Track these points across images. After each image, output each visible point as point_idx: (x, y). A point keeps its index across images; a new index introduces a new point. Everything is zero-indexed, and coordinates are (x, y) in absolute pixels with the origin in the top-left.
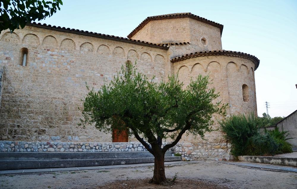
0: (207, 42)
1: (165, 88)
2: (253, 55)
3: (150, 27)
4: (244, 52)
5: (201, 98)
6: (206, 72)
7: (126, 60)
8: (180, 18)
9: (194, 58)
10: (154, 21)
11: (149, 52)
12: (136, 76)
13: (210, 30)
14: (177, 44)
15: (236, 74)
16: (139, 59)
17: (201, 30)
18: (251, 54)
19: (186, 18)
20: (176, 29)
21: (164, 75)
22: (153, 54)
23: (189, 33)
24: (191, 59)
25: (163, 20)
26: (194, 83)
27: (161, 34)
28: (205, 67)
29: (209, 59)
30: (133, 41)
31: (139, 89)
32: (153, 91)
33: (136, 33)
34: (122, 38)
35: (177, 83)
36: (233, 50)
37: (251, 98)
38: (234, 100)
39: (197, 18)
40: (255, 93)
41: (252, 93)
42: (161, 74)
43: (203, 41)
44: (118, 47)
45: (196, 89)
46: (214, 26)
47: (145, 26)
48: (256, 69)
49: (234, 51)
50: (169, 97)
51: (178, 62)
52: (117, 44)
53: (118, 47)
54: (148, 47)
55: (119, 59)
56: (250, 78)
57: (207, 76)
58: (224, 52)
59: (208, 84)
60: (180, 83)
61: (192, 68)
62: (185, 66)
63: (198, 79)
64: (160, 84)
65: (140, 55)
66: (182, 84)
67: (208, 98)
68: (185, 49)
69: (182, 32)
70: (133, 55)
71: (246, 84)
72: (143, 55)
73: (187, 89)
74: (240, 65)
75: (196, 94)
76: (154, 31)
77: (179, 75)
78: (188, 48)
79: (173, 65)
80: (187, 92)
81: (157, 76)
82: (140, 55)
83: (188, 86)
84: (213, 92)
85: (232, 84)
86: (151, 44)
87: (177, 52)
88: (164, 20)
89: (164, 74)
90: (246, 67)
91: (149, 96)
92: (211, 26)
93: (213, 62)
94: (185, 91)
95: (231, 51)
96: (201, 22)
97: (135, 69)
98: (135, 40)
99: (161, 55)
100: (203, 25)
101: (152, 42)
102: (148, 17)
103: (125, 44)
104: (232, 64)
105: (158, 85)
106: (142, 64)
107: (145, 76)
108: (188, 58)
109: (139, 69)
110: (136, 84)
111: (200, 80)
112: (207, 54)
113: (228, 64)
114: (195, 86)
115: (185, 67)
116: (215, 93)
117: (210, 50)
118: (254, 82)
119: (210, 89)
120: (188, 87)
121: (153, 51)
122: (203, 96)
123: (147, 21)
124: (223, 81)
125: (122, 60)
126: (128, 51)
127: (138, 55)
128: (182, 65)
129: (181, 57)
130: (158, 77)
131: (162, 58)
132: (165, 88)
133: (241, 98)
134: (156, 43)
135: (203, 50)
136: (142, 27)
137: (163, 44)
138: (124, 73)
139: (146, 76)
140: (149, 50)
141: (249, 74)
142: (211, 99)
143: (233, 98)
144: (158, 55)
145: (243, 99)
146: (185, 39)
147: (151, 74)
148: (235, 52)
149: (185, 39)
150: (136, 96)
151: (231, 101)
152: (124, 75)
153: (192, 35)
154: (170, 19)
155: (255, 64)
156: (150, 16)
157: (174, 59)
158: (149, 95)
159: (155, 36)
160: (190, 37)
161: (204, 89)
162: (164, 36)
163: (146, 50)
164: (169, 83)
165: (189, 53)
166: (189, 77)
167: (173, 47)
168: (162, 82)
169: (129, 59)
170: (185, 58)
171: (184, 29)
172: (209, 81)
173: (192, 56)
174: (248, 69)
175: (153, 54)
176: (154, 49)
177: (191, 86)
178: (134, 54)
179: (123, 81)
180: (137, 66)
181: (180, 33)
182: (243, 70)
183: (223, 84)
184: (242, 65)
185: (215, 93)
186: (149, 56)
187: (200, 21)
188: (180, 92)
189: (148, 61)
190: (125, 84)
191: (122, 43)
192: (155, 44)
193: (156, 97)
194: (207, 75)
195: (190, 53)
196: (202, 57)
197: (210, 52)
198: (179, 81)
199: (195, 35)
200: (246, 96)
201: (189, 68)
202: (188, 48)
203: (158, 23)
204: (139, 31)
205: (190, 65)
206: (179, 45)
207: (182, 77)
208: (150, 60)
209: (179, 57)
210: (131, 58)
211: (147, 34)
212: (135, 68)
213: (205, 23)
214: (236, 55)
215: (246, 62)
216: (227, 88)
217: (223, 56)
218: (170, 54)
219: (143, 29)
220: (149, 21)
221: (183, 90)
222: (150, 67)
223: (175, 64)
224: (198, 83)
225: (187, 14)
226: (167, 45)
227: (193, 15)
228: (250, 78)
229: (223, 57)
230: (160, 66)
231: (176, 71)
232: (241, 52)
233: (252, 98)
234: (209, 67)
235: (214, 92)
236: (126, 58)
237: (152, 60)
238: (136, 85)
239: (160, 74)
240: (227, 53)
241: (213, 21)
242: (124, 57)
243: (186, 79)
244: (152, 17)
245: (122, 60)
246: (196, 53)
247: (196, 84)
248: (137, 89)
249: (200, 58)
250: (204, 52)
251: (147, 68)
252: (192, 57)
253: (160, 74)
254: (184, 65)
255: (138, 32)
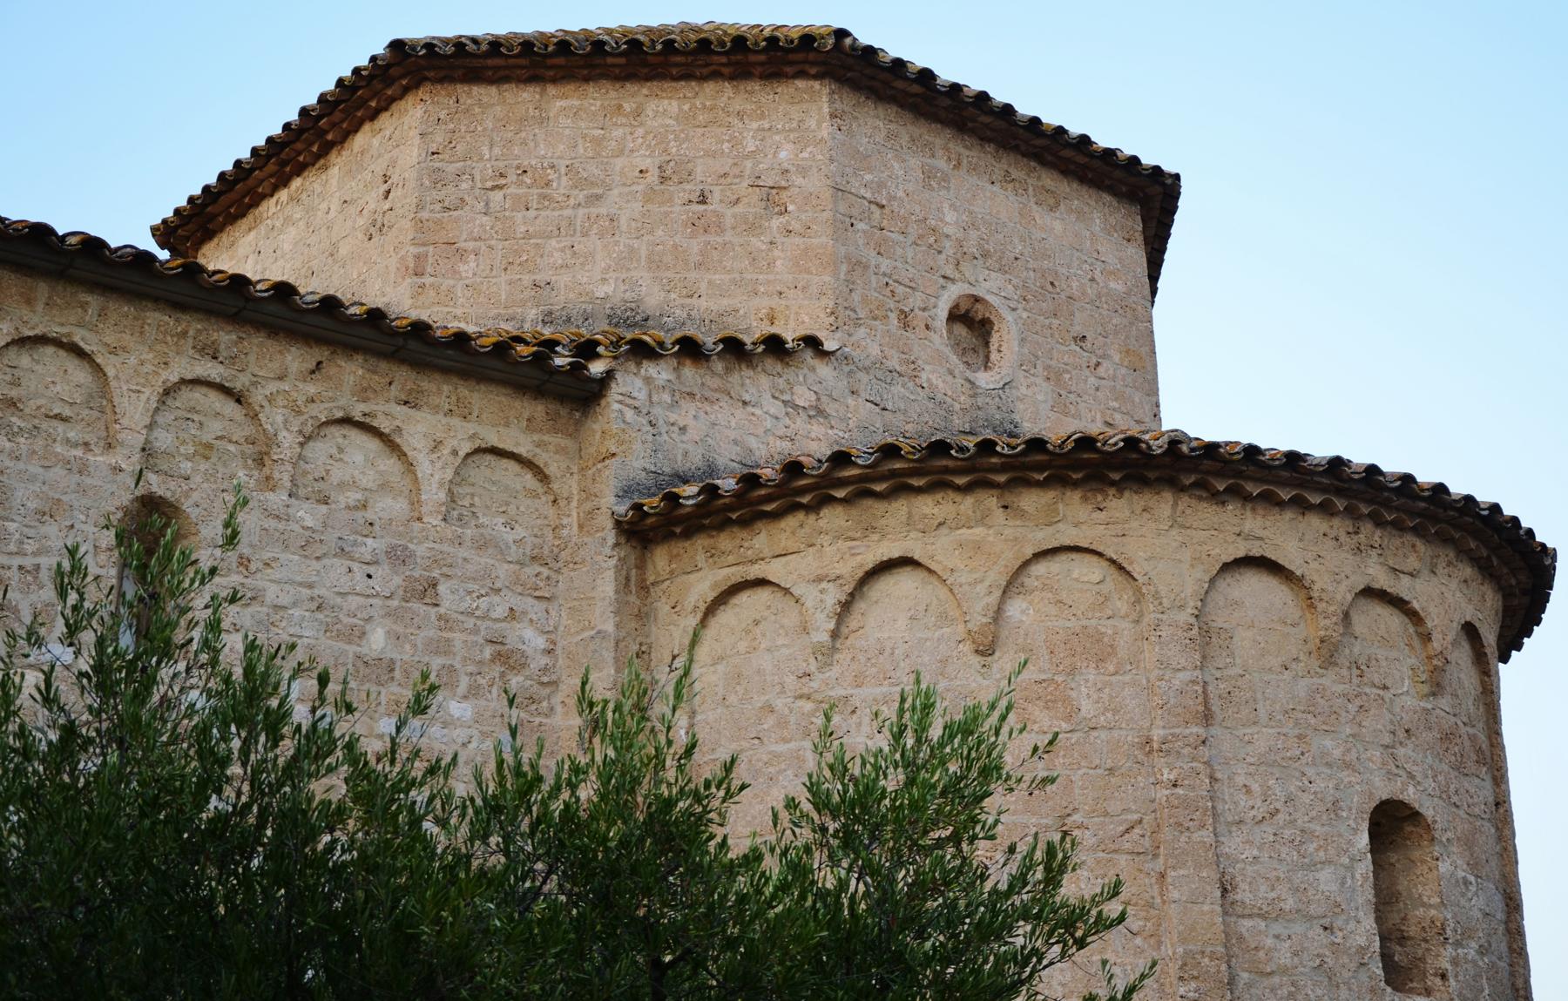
0: (1007, 340)
1: (544, 817)
2: (1484, 496)
3: (411, 155)
4: (1391, 464)
5: (922, 936)
6: (986, 651)
7: (121, 495)
8: (732, 78)
9: (869, 502)
10: (461, 89)
11: (388, 413)
12: (227, 680)
13: (1041, 216)
14: (690, 349)
15: (1302, 688)
16: (269, 483)
17: (950, 217)
18: (1457, 488)
19: (800, 83)
20: (691, 188)
21: (545, 670)
22: (437, 445)
23: (822, 239)
24: (832, 517)
25: (552, 90)
26: (856, 770)
27: (527, 235)
28: (981, 603)
29: (1022, 514)
30: (215, 288)
31: (252, 820)
32: (409, 850)
33: (255, 204)
34: (93, 246)
35: (671, 775)
36: (1275, 438)
37: (1471, 950)
38: (1284, 971)
39: (916, 89)
40: (1512, 904)
41: (1481, 901)
42: (508, 659)
43: (961, 330)
44: (42, 340)
45: (873, 838)
46: (1083, 180)
47: (360, 140)
48: (1511, 641)
49: (1285, 446)
50: (579, 924)
51: (701, 542)
52: (29, 302)
53: (42, 340)
54: (383, 366)
55: (34, 469)
56: (1447, 737)
57: (993, 707)
58: (1182, 456)
59: (997, 788)
60: (705, 766)
61: (846, 606)
62: (761, 582)
63: (898, 735)
64: (490, 770)
65: (288, 440)
66: (727, 780)
67: (999, 938)
68: (775, 408)
69: (753, 227)
70: (207, 437)
71: (1410, 795)
72: (319, 451)
73: (772, 838)
74: (1343, 593)
75: (867, 894)
76: (450, 194)
77: (706, 676)
78: (804, 397)
79: (641, 566)
80: (772, 865)
81: (464, 682)
82: (288, 440)
83: (791, 804)
84: (1053, 878)
85: (1255, 787)
86: (420, 329)
87: (692, 434)
88: (569, 88)
89: (544, 660)
90: (1414, 616)
91: (350, 910)
92: (1049, 179)
93: (1063, 558)
94: (753, 858)
95: (1252, 451)
96: (948, 132)
97: (215, 603)
98: (239, 283)
99: (522, 450)
100: (973, 169)
101: (424, 316)
102: (397, 46)
103: (122, 310)
104: (1254, 588)
105: (462, 787)
106: (308, 544)
107: (323, 680)
108: (805, 500)
109: (272, 593)
110: (225, 762)
111: (919, 741)
112: (1002, 469)
113: (1222, 584)
114: (867, 794)
115: (763, 595)
116: (1073, 888)
117: (1029, 429)
118: (1499, 776)
119: (1022, 848)
120: (784, 816)
121: (436, 409)
122: (950, 919)
123: (390, 82)
124: (1160, 761)
125: (82, 490)
126: (150, 395)
127: (271, 440)
128: (736, 574)
129: (728, 484)
130: (473, 692)
131: (534, 495)
132: (544, 817)
133: (1362, 950)
134: (471, 329)
135: (959, 427)
136: (326, 149)
137: (551, 344)
138: (88, 637)
139: (336, 676)
140: (394, 391)
141: (1436, 687)
142: (1035, 952)
143: (1269, 942)
144: (489, 458)
145: (1386, 957)
146: (775, 302)
147: (404, 654)
148: (1293, 458)
149: (775, 302)
150: (209, 903)
151: (1245, 975)
152: (84, 665)
153: (857, 265)
154: (631, 87)
155: (1506, 593)
156: (418, 28)
157: (652, 503)
158: (360, 894)
159: (462, 254)
160: (827, 278)
161: (955, 839)
162: (558, 258)
163: (363, 393)
164: (583, 760)
165: (815, 444)
166: (808, 706)
167: (648, 380)
168: (509, 758)
169: (155, 484)
170: (769, 499)
171: (772, 197)
172: (1013, 755)
173: (842, 483)
174: (1426, 638)
175: (437, 445)
176: (442, 391)
177: (821, 801)
178: (215, 427)
179: (69, 731)
180: (244, 562)
181: (728, 236)
182: (1381, 653)
183: (1162, 793)
184: (1369, 593)
185: (1073, 888)
186: (390, 464)
187: (945, 122)
188: (696, 870)
189: (370, 516)
190: (88, 764)
191: (94, 301)
192: (461, 338)
193: (438, 920)
194: (991, 697)
195: (824, 451)
196: (951, 494)
197: (1037, 444)
198: (689, 751)
199: (885, 265)
200: (1413, 930)
201: (809, 604)
202: (804, 397)
203: (499, 110)
204: (296, 183)
205: (819, 579)
206: (719, 366)
207: (732, 699)
208: (390, 507)
209: (711, 491)
210: (186, 466)
211: (377, 228)
212: (222, 585)
213: (990, 148)
214: (1301, 485)
215: (1412, 562)
216: (1206, 836)
217: (1168, 496)
218: (613, 449)
219: (339, 162)
220: (406, 91)
221: (737, 850)
222: (388, 579)
223: (660, 559)
224: (893, 781)
225: (808, 39)
226: (587, 350)
227: (870, 51)
228: (1447, 737)
229: (1164, 504)
230: (503, 571)
231: (671, 633)
232: (1359, 456)
233: (1482, 951)
234: (1016, 609)
235: (1066, 879)
236: (131, 464)
237: (415, 502)
238: (212, 781)
239: (499, 657)
240: (1207, 464)
241: (1075, 129)
242: (99, 459)
243: (770, 721)
244: (471, 47)
245: (82, 490)
246: (890, 451)
247: (869, 790)
248: (220, 818)
249: (928, 506)
250: (970, 443)
251: (361, 584)
252: (840, 494)
253: (499, 657)
254: (755, 572)
255: (283, 195)
